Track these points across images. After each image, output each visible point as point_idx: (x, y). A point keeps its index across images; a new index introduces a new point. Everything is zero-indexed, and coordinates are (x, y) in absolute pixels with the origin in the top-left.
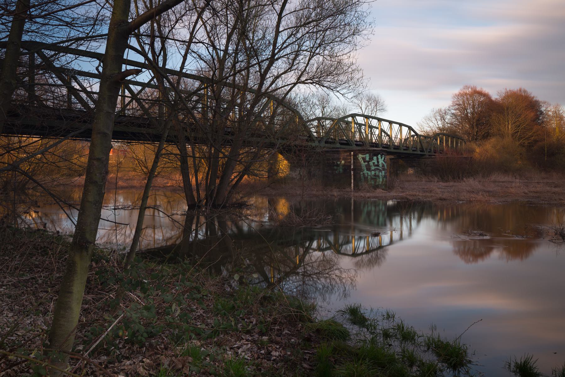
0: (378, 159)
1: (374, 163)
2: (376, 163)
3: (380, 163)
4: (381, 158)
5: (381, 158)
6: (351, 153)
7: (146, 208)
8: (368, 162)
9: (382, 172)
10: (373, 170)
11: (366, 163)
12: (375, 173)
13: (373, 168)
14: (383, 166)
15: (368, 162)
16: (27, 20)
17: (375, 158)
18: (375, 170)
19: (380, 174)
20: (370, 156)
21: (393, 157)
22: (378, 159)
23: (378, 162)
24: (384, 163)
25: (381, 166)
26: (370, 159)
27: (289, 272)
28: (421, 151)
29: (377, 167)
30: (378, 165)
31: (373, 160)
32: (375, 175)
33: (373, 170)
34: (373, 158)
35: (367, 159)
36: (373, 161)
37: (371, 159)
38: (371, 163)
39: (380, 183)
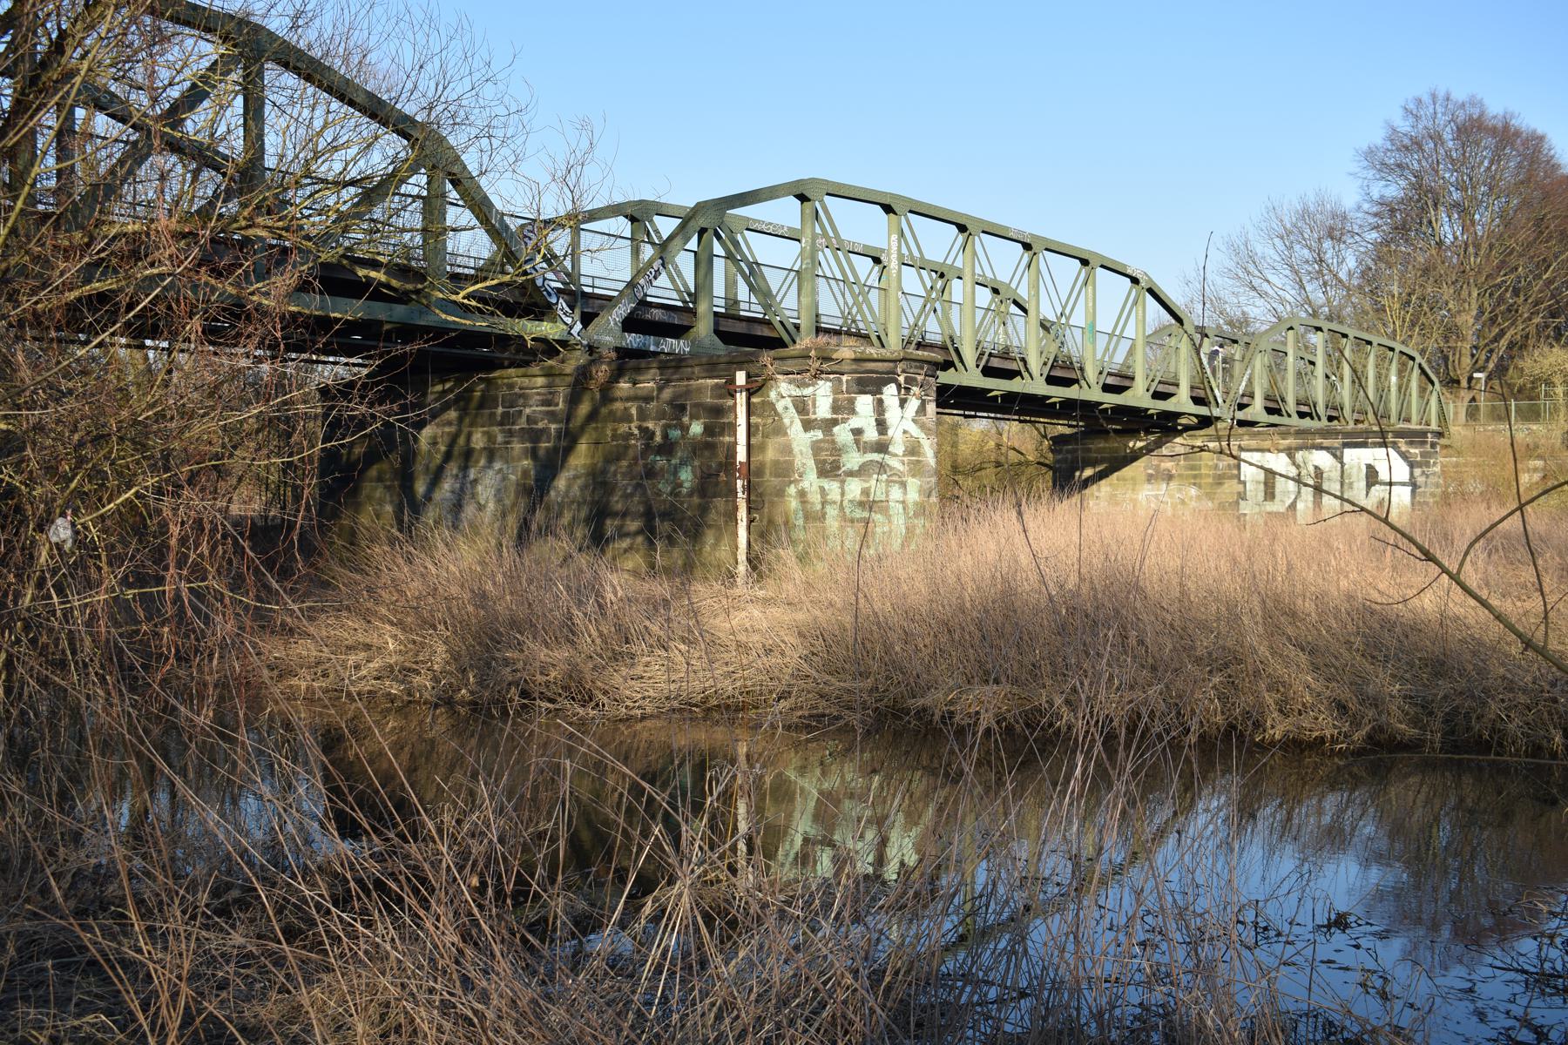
0: (880, 407)
1: (857, 432)
2: (871, 434)
3: (895, 433)
4: (903, 403)
5: (903, 403)
6: (732, 381)
7: (1544, 647)
8: (829, 424)
9: (903, 485)
10: (851, 474)
11: (819, 435)
12: (866, 492)
13: (853, 460)
14: (913, 449)
15: (829, 424)
16: (423, 171)
17: (864, 403)
18: (862, 472)
19: (896, 493)
20: (836, 390)
21: (1062, 429)
22: (880, 407)
23: (881, 425)
24: (915, 431)
25: (898, 448)
26: (836, 408)
27: (1399, 746)
28: (1198, 401)
29: (876, 457)
30: (882, 447)
31: (853, 411)
32: (868, 504)
33: (851, 474)
34: (852, 402)
35: (823, 410)
36: (855, 422)
37: (843, 408)
38: (842, 434)
39: (896, 544)
